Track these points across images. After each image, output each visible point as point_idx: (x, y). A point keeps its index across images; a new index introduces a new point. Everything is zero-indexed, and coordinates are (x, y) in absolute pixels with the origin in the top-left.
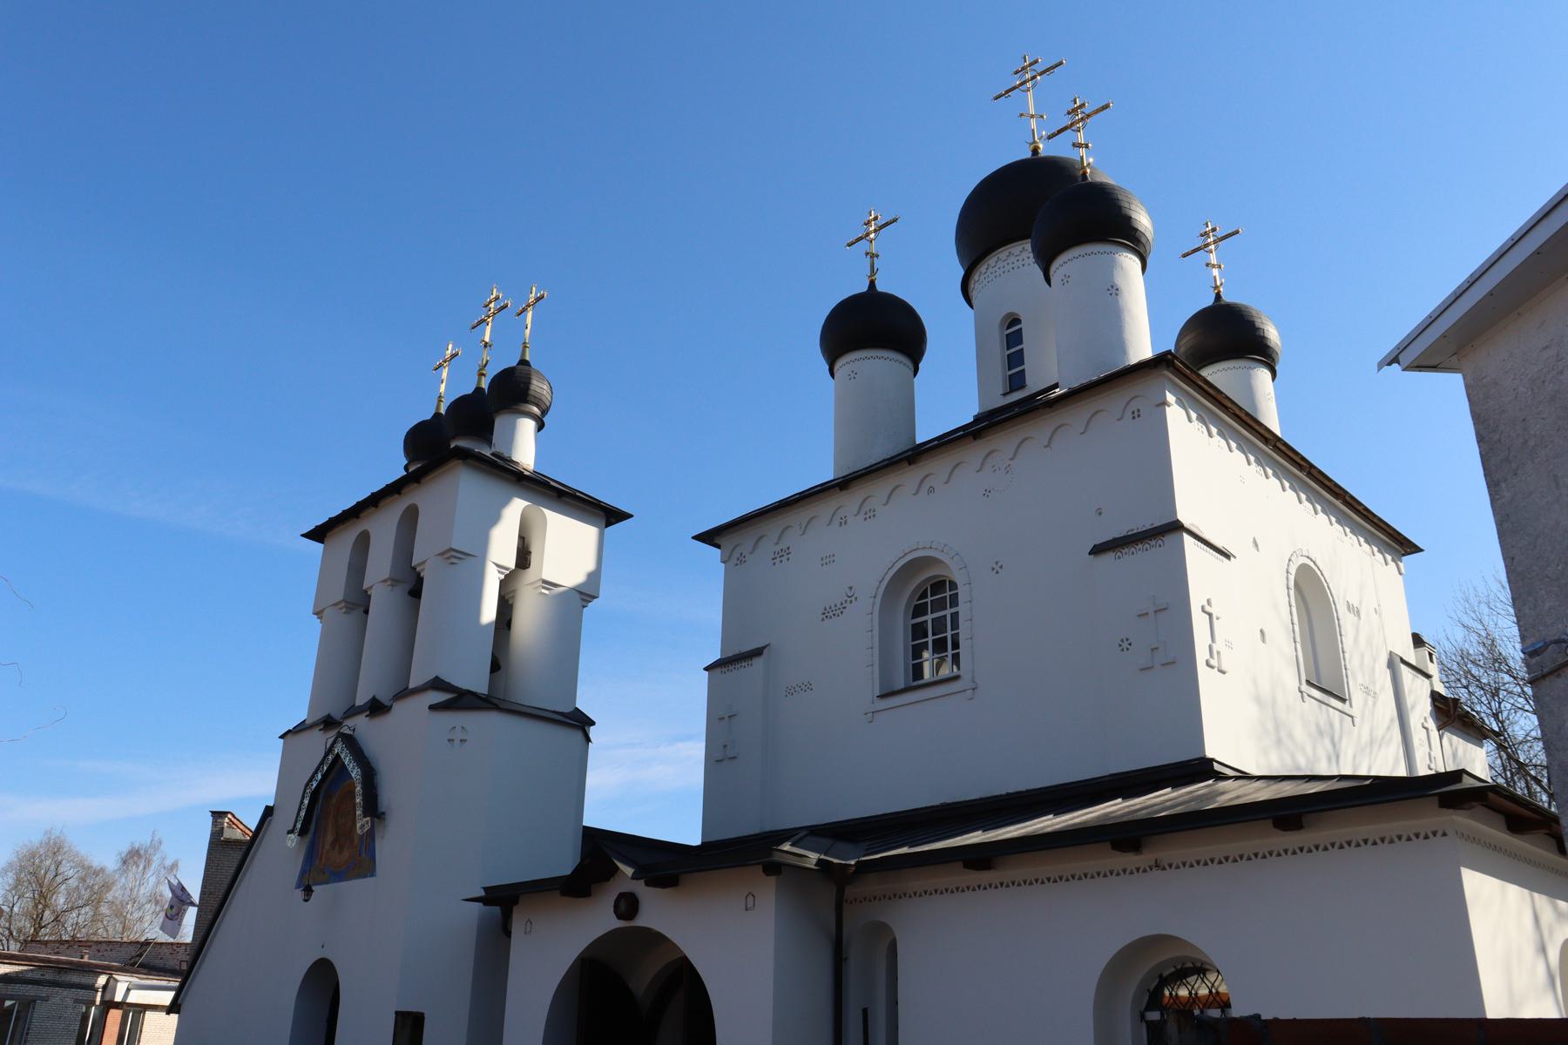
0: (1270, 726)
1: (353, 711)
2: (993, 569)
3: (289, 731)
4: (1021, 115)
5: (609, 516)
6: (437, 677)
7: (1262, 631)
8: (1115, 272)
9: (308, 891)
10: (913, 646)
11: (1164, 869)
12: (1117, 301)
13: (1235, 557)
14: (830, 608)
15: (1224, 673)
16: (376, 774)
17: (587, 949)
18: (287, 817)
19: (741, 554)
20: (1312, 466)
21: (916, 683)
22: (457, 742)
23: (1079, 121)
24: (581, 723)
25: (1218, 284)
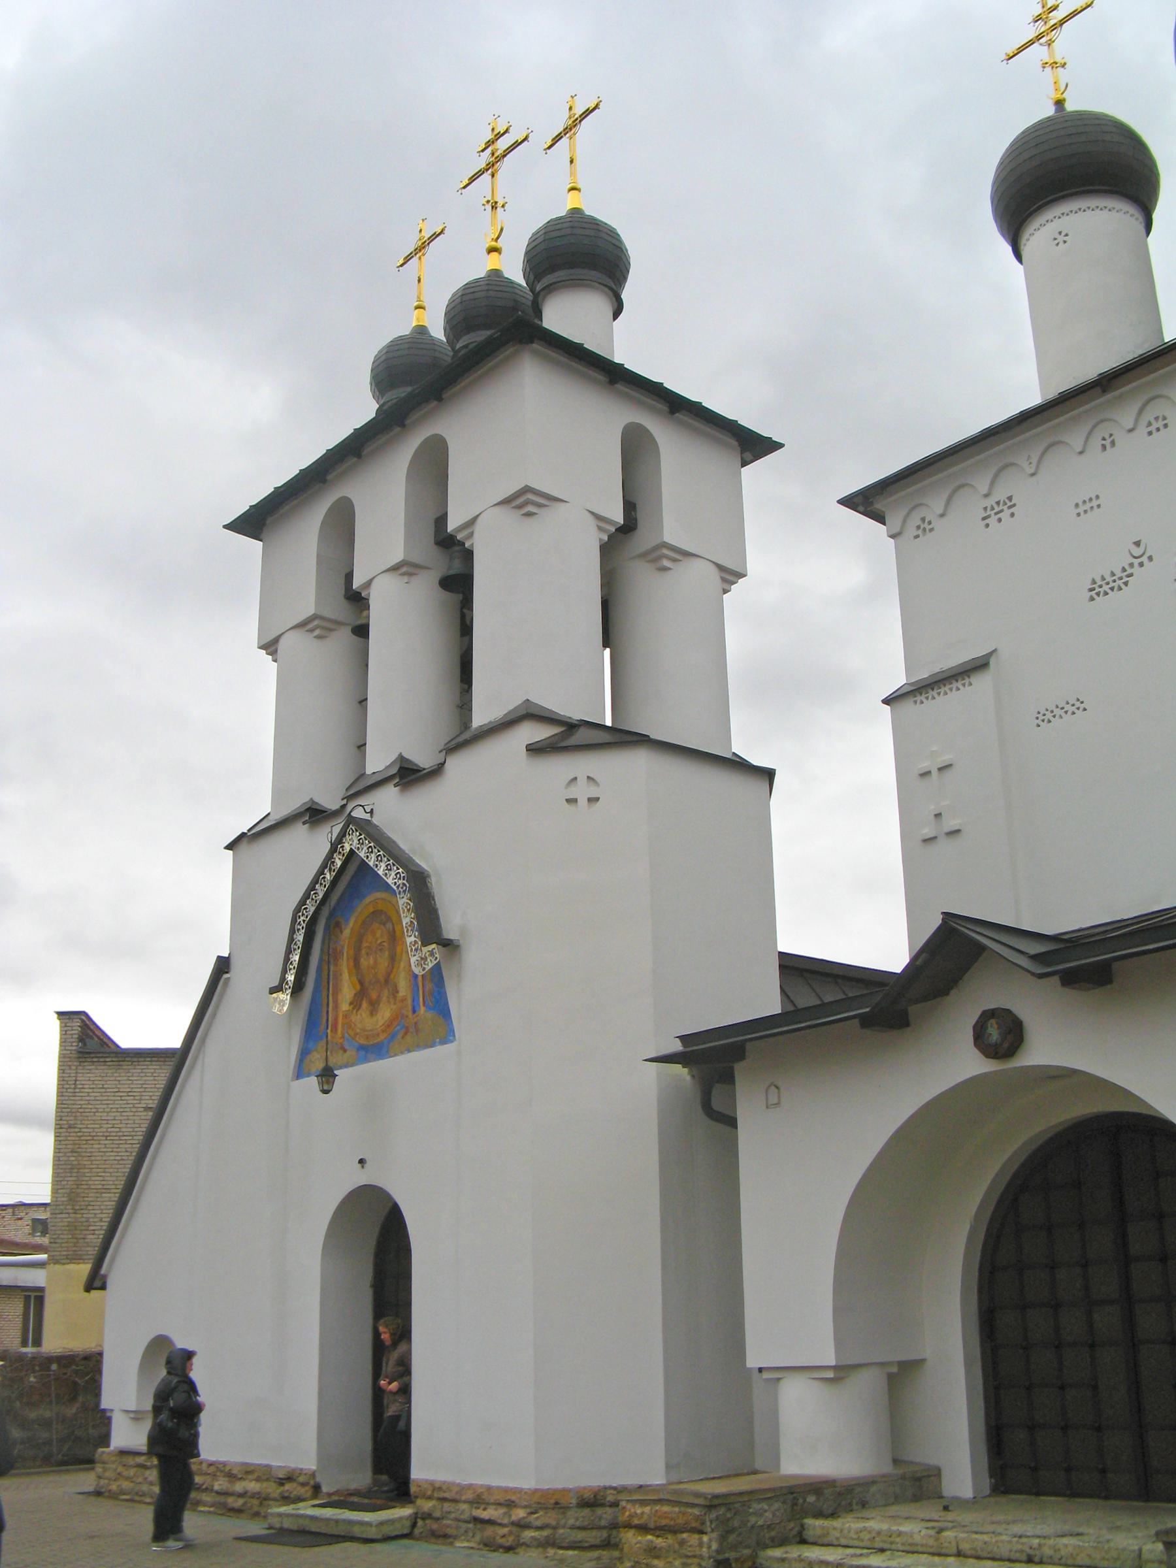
1: (362, 786)
3: (243, 835)
9: (327, 1077)
19: (923, 520)
22: (582, 801)
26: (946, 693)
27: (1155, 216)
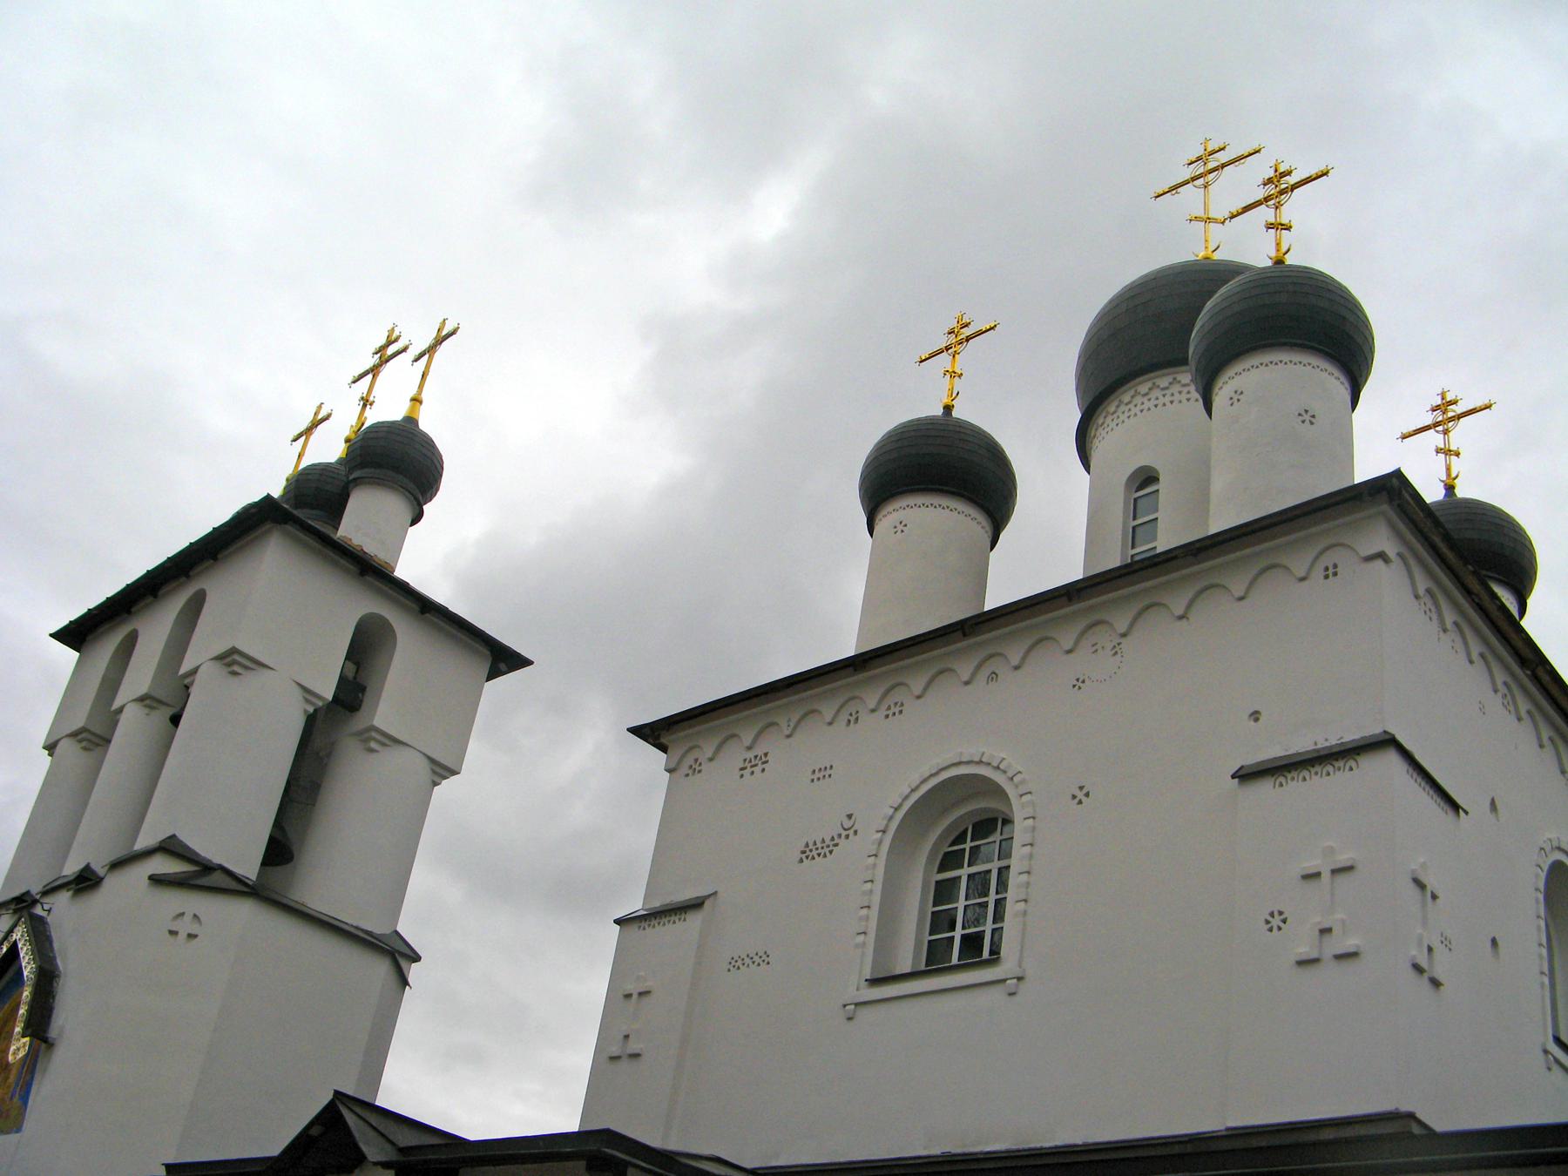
2: (1074, 686)
14: (815, 843)
19: (696, 760)
22: (182, 935)
26: (674, 922)
27: (1529, 601)
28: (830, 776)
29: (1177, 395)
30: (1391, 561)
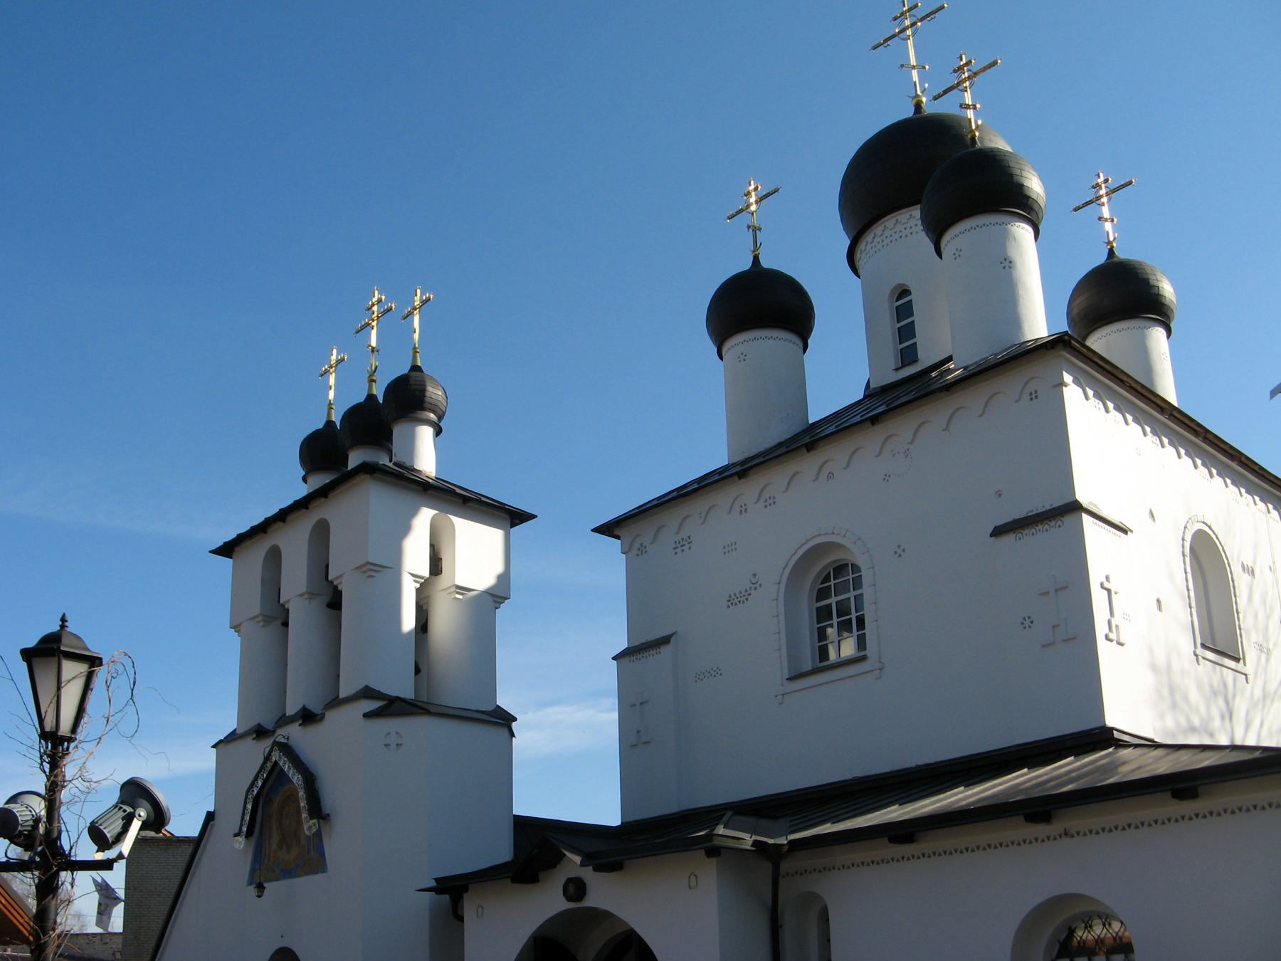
0: (1165, 692)
1: (284, 721)
4: (902, 66)
5: (512, 517)
6: (367, 686)
7: (1158, 601)
8: (1008, 244)
9: (260, 887)
10: (818, 628)
11: (1073, 836)
12: (1011, 274)
13: (1132, 531)
14: (735, 595)
15: (1122, 644)
16: (316, 779)
17: (539, 928)
18: (232, 819)
19: (642, 545)
20: (1207, 431)
21: (823, 664)
22: (393, 746)
23: (965, 80)
24: (504, 720)
25: (1111, 239)
27: (809, 341)
28: (736, 549)
29: (914, 228)
30: (1069, 385)
